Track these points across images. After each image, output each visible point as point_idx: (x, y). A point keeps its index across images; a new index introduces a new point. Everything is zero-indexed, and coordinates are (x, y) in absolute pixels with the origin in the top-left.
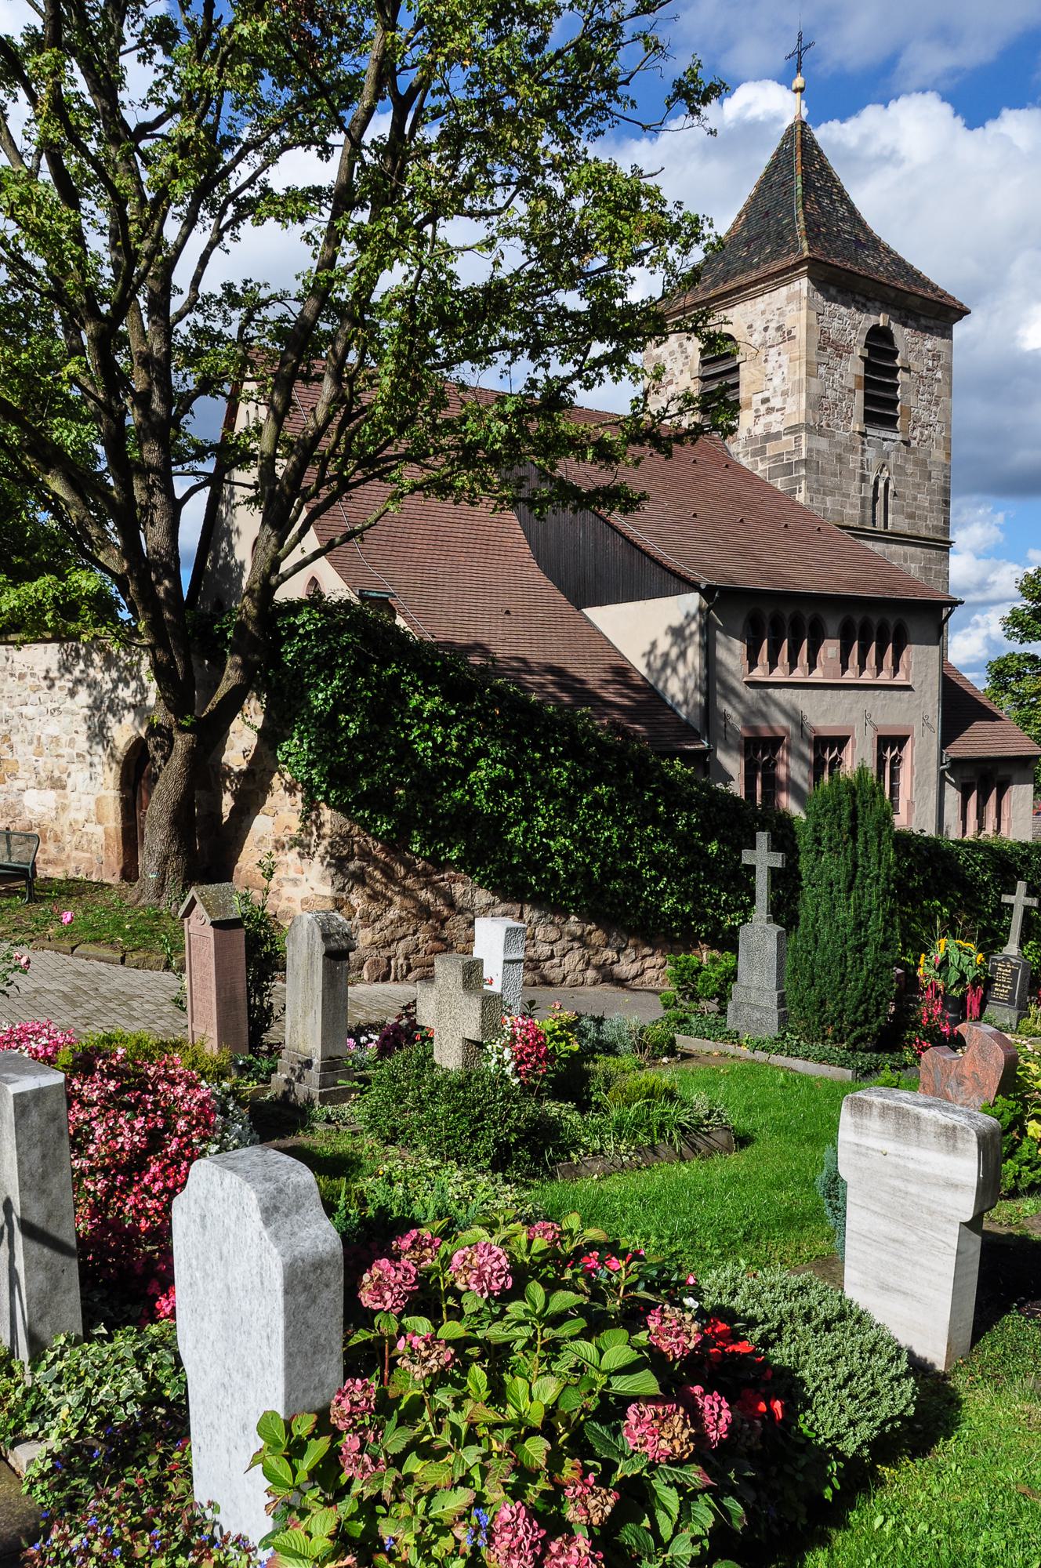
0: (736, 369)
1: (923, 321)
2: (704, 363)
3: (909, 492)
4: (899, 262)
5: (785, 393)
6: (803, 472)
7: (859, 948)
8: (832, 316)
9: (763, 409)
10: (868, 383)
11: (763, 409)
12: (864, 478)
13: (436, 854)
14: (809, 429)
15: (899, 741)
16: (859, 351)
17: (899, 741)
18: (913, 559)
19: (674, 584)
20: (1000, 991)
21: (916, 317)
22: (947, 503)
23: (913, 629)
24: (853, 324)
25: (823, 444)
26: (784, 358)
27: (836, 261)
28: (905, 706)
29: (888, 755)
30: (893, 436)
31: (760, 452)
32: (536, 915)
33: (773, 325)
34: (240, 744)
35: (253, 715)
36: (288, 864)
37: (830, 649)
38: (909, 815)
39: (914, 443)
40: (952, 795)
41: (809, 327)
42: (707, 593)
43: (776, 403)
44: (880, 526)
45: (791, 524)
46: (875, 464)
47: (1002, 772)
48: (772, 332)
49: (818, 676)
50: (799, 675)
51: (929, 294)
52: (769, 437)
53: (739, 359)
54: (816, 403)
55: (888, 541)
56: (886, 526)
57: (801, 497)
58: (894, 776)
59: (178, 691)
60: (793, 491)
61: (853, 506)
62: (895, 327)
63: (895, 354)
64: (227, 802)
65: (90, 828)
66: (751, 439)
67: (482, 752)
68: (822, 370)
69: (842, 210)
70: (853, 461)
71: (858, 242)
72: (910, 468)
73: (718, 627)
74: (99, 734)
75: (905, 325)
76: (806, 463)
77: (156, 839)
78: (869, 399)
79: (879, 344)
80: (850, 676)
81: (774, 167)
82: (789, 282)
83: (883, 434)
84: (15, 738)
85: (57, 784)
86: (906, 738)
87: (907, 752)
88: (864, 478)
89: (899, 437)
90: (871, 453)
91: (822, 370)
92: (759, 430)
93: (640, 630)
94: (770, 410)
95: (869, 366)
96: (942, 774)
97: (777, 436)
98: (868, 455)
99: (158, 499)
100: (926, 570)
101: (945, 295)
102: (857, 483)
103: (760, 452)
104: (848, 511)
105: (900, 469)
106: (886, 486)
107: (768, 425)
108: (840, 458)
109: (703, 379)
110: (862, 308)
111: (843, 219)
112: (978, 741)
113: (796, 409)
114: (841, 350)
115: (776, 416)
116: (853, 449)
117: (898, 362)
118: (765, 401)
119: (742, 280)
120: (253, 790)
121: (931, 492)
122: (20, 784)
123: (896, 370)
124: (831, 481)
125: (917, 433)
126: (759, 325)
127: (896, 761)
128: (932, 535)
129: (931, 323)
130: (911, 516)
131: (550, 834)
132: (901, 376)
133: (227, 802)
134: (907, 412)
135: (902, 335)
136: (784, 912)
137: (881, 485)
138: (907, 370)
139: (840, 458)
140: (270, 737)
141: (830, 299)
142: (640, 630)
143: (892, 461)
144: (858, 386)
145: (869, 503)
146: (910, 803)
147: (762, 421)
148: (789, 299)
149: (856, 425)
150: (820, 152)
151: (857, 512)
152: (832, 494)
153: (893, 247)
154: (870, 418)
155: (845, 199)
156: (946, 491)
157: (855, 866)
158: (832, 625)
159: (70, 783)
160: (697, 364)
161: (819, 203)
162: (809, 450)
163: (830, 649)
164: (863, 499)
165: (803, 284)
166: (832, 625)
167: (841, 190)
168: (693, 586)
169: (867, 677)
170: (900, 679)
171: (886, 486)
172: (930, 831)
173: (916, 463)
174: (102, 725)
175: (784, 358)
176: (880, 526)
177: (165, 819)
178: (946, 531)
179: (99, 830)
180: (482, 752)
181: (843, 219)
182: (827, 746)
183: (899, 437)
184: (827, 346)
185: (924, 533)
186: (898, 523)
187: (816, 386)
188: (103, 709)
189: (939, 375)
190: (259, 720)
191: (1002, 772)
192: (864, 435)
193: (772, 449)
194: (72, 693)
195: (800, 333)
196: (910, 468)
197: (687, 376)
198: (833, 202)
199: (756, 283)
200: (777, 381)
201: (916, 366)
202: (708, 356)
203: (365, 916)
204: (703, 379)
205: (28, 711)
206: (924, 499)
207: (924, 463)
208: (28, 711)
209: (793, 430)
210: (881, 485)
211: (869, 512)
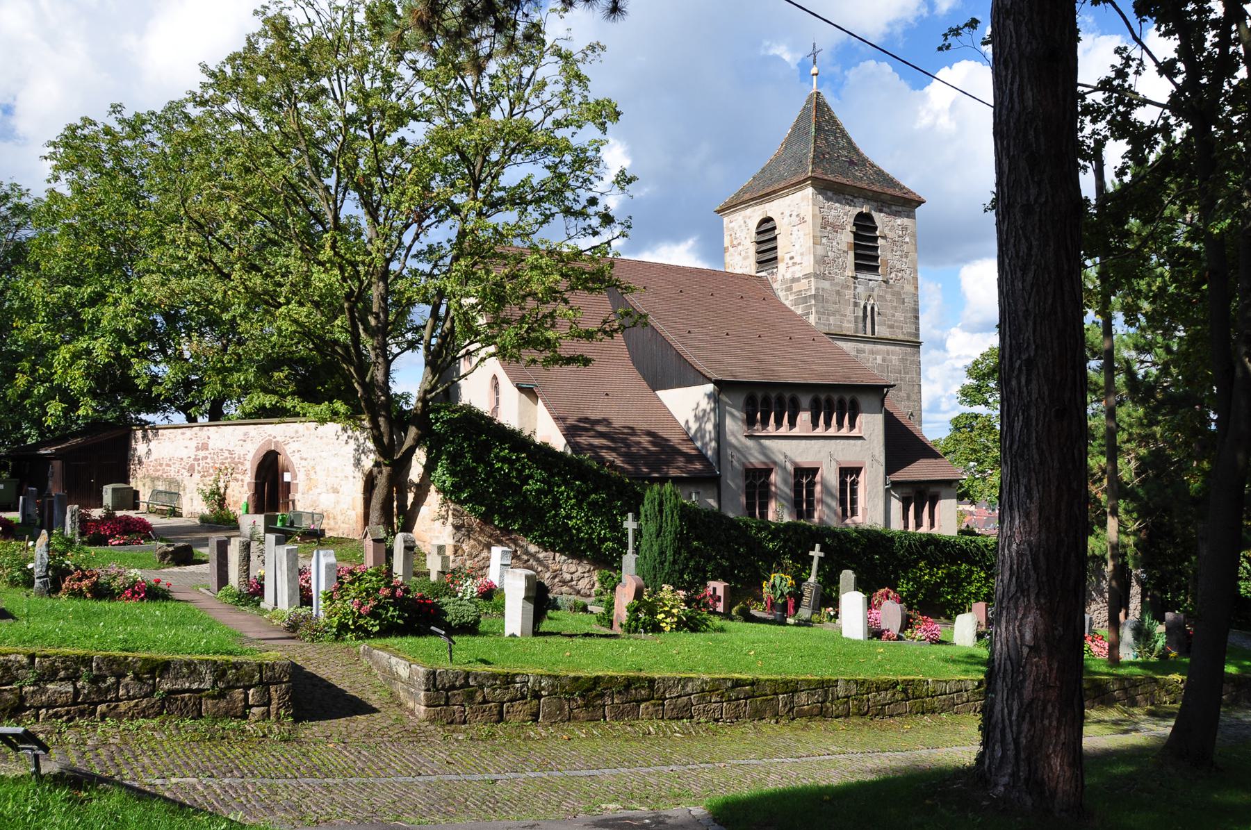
0: (775, 238)
1: (894, 208)
2: (758, 233)
3: (889, 312)
4: (880, 174)
5: (802, 254)
6: (813, 302)
7: (662, 563)
8: (830, 209)
9: (790, 262)
10: (856, 246)
11: (790, 262)
12: (856, 304)
13: (506, 526)
14: (816, 276)
15: (857, 471)
16: (850, 228)
17: (857, 471)
18: (893, 353)
19: (701, 379)
20: (805, 601)
21: (889, 206)
22: (917, 318)
23: (863, 400)
24: (846, 214)
25: (826, 284)
26: (801, 233)
27: (831, 177)
28: (858, 449)
29: (849, 480)
30: (876, 278)
31: (789, 289)
32: (563, 557)
33: (794, 214)
34: (416, 472)
35: (420, 457)
36: (434, 527)
37: (804, 417)
38: (864, 517)
39: (891, 282)
40: (896, 506)
41: (814, 216)
42: (716, 383)
43: (797, 259)
44: (869, 334)
45: (795, 336)
46: (864, 295)
47: (933, 490)
48: (794, 217)
49: (796, 431)
50: (784, 431)
51: (897, 192)
52: (794, 280)
53: (777, 232)
54: (821, 261)
55: (874, 343)
56: (873, 333)
57: (812, 319)
58: (854, 492)
59: (384, 450)
60: (808, 314)
61: (849, 322)
62: (874, 214)
63: (876, 228)
64: (411, 497)
65: (349, 512)
66: (784, 281)
67: (531, 476)
68: (824, 240)
69: (843, 143)
70: (849, 294)
71: (852, 163)
72: (889, 297)
73: (727, 404)
74: (358, 463)
75: (881, 211)
76: (815, 296)
77: (375, 515)
78: (857, 256)
79: (864, 226)
80: (820, 431)
81: (800, 119)
82: (801, 189)
83: (869, 277)
84: (317, 468)
85: (336, 491)
86: (861, 469)
87: (861, 478)
88: (856, 304)
89: (880, 278)
90: (860, 289)
91: (824, 240)
92: (788, 276)
93: (686, 405)
94: (794, 264)
95: (857, 236)
96: (887, 491)
97: (798, 280)
98: (858, 290)
99: (380, 360)
100: (903, 360)
101: (909, 192)
102: (851, 307)
103: (789, 289)
104: (846, 325)
105: (882, 298)
106: (873, 308)
107: (794, 273)
108: (838, 293)
109: (758, 243)
110: (850, 203)
111: (843, 148)
112: (919, 471)
113: (808, 265)
114: (837, 228)
115: (797, 267)
116: (848, 287)
117: (878, 233)
118: (792, 258)
119: (777, 187)
120: (421, 492)
121: (905, 311)
122: (319, 491)
123: (876, 238)
124: (832, 308)
125: (893, 275)
126: (787, 213)
127: (854, 484)
128: (907, 338)
129: (900, 209)
130: (891, 327)
131: (569, 517)
132: (880, 241)
133: (411, 497)
134: (886, 263)
135: (879, 218)
136: (637, 550)
137: (869, 308)
138: (884, 237)
139: (838, 293)
140: (429, 468)
141: (829, 199)
142: (686, 405)
143: (875, 294)
144: (850, 249)
145: (861, 319)
146: (865, 509)
147: (791, 270)
148: (803, 199)
149: (850, 272)
150: (829, 109)
151: (852, 325)
152: (834, 314)
153: (877, 163)
154: (858, 267)
155: (844, 135)
156: (916, 311)
157: (661, 527)
158: (805, 400)
159: (341, 490)
160: (754, 234)
161: (826, 139)
162: (817, 289)
163: (804, 417)
164: (856, 317)
165: (809, 191)
166: (805, 400)
167: (842, 131)
168: (710, 381)
169: (832, 431)
170: (855, 433)
171: (873, 308)
172: (879, 524)
173: (893, 294)
174: (359, 460)
175: (801, 233)
176: (869, 334)
177: (378, 506)
178: (917, 335)
179: (353, 513)
180: (531, 476)
181: (843, 148)
182: (804, 476)
183: (880, 278)
184: (827, 226)
185: (901, 337)
186: (881, 331)
187: (820, 250)
188: (360, 450)
189: (907, 239)
190: (424, 461)
191: (933, 490)
192: (855, 278)
193: (796, 287)
194: (347, 443)
195: (809, 219)
196: (889, 297)
197: (749, 241)
198: (836, 138)
199: (783, 189)
200: (797, 246)
201: (890, 235)
202: (762, 229)
203: (470, 555)
204: (758, 243)
205: (323, 454)
206: (900, 316)
207: (899, 293)
208: (323, 454)
209: (807, 276)
210: (869, 308)
211: (861, 325)
